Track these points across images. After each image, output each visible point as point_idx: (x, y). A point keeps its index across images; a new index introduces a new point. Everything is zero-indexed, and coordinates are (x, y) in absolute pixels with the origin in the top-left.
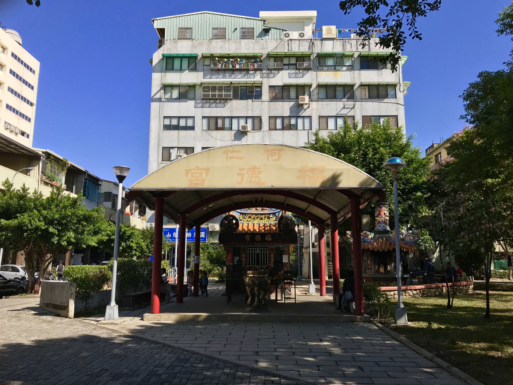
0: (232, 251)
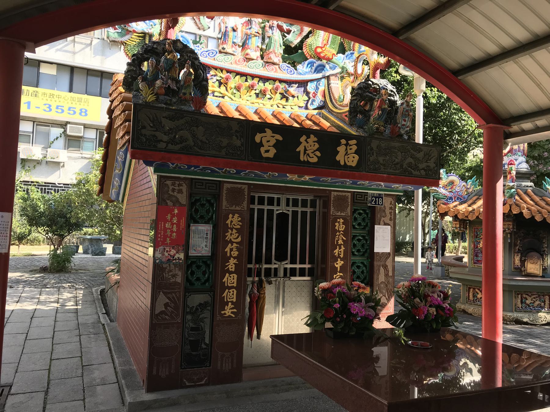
0: (183, 199)
